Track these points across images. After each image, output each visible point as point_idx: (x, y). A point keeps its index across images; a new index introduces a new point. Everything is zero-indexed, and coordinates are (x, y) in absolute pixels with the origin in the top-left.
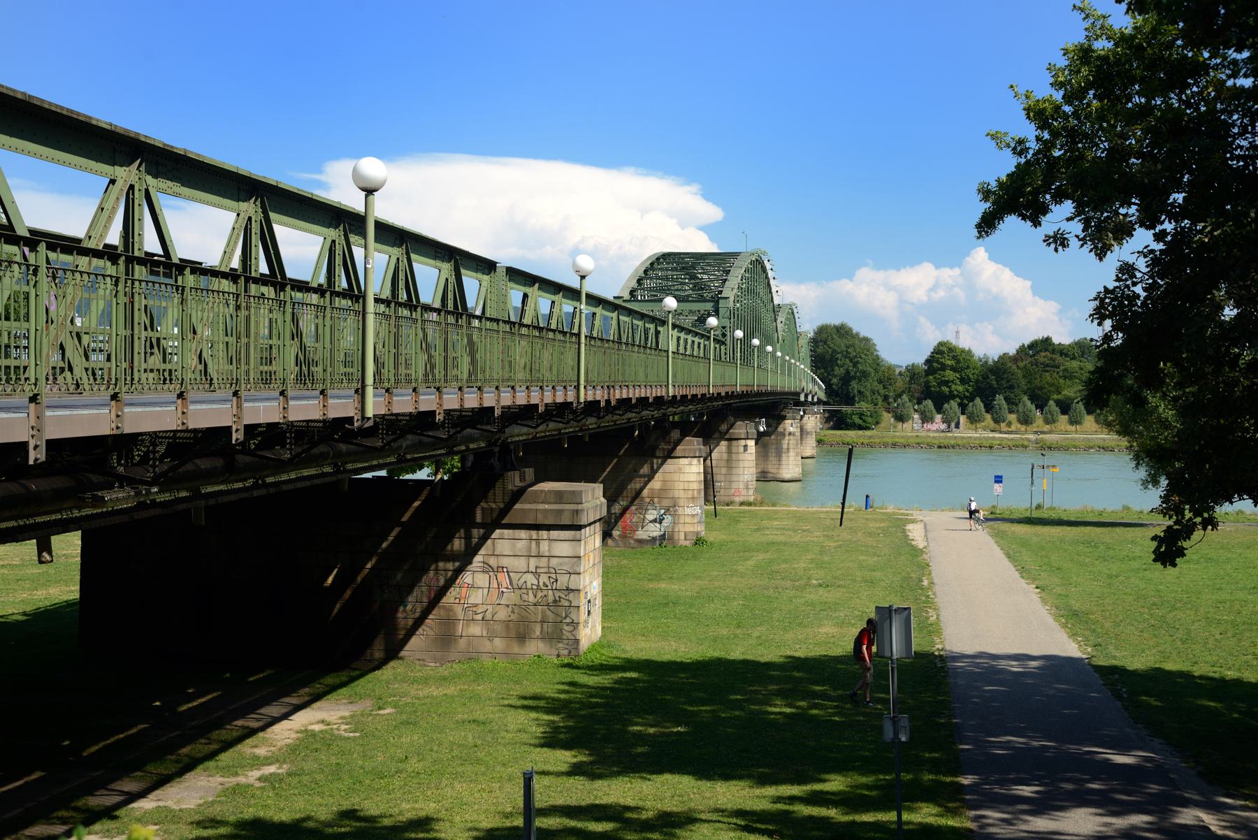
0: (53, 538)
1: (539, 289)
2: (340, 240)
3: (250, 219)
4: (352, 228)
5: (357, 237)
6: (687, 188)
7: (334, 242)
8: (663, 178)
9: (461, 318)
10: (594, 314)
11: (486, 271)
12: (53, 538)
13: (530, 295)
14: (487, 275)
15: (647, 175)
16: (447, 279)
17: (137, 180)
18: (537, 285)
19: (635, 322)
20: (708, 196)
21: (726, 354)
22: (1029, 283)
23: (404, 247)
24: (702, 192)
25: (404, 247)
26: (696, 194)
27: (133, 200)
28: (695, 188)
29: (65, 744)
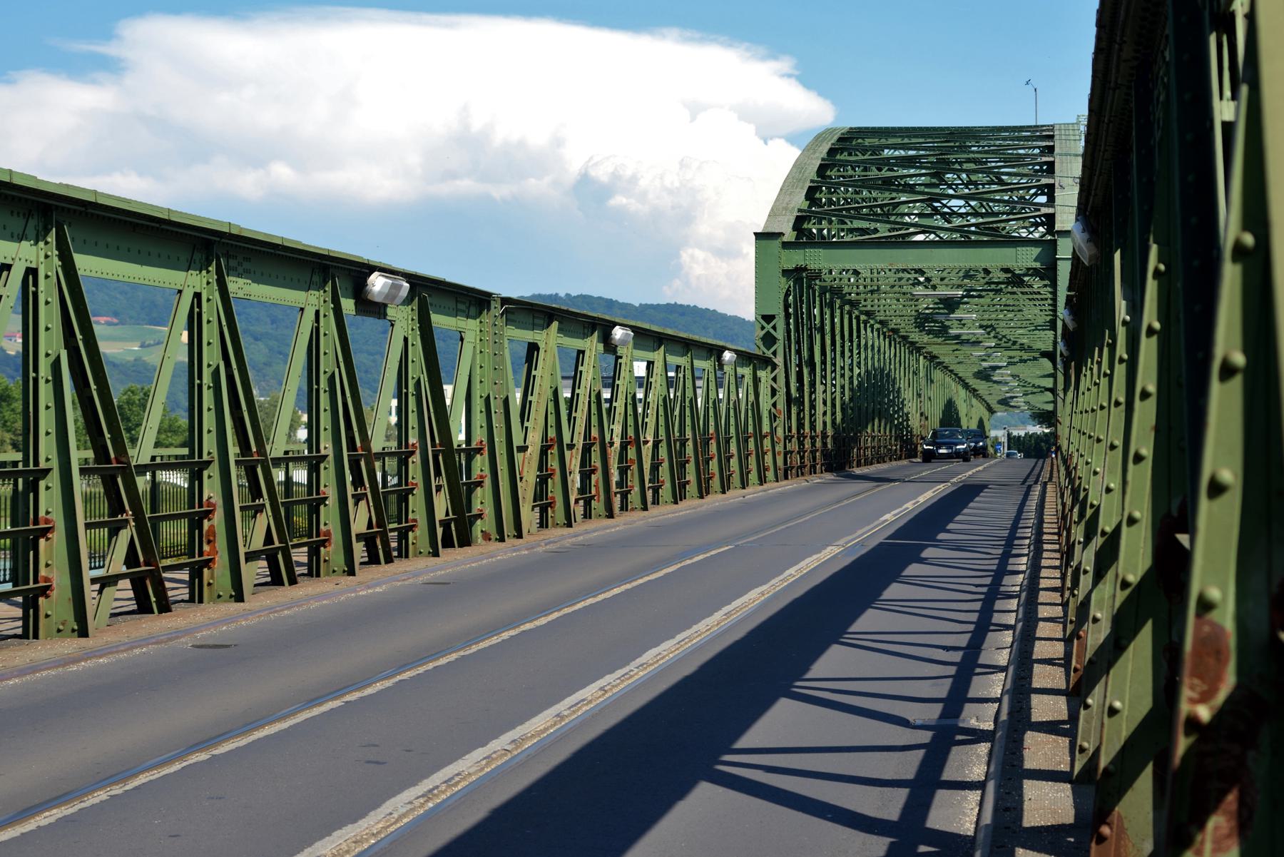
0: (1033, 720)
1: (560, 330)
2: (47, 268)
3: (198, 296)
4: (233, 263)
5: (241, 281)
6: (773, 65)
7: (198, 296)
8: (730, 46)
9: (790, 441)
10: (533, 348)
11: (473, 311)
12: (1033, 720)
13: (542, 345)
14: (475, 318)
15: (701, 41)
16: (406, 340)
17: (42, 259)
18: (555, 325)
19: (697, 363)
20: (808, 78)
21: (774, 392)
23: (212, 268)
24: (797, 73)
25: (328, 288)
26: (790, 76)
27: (36, 295)
28: (785, 64)
29: (1069, 839)
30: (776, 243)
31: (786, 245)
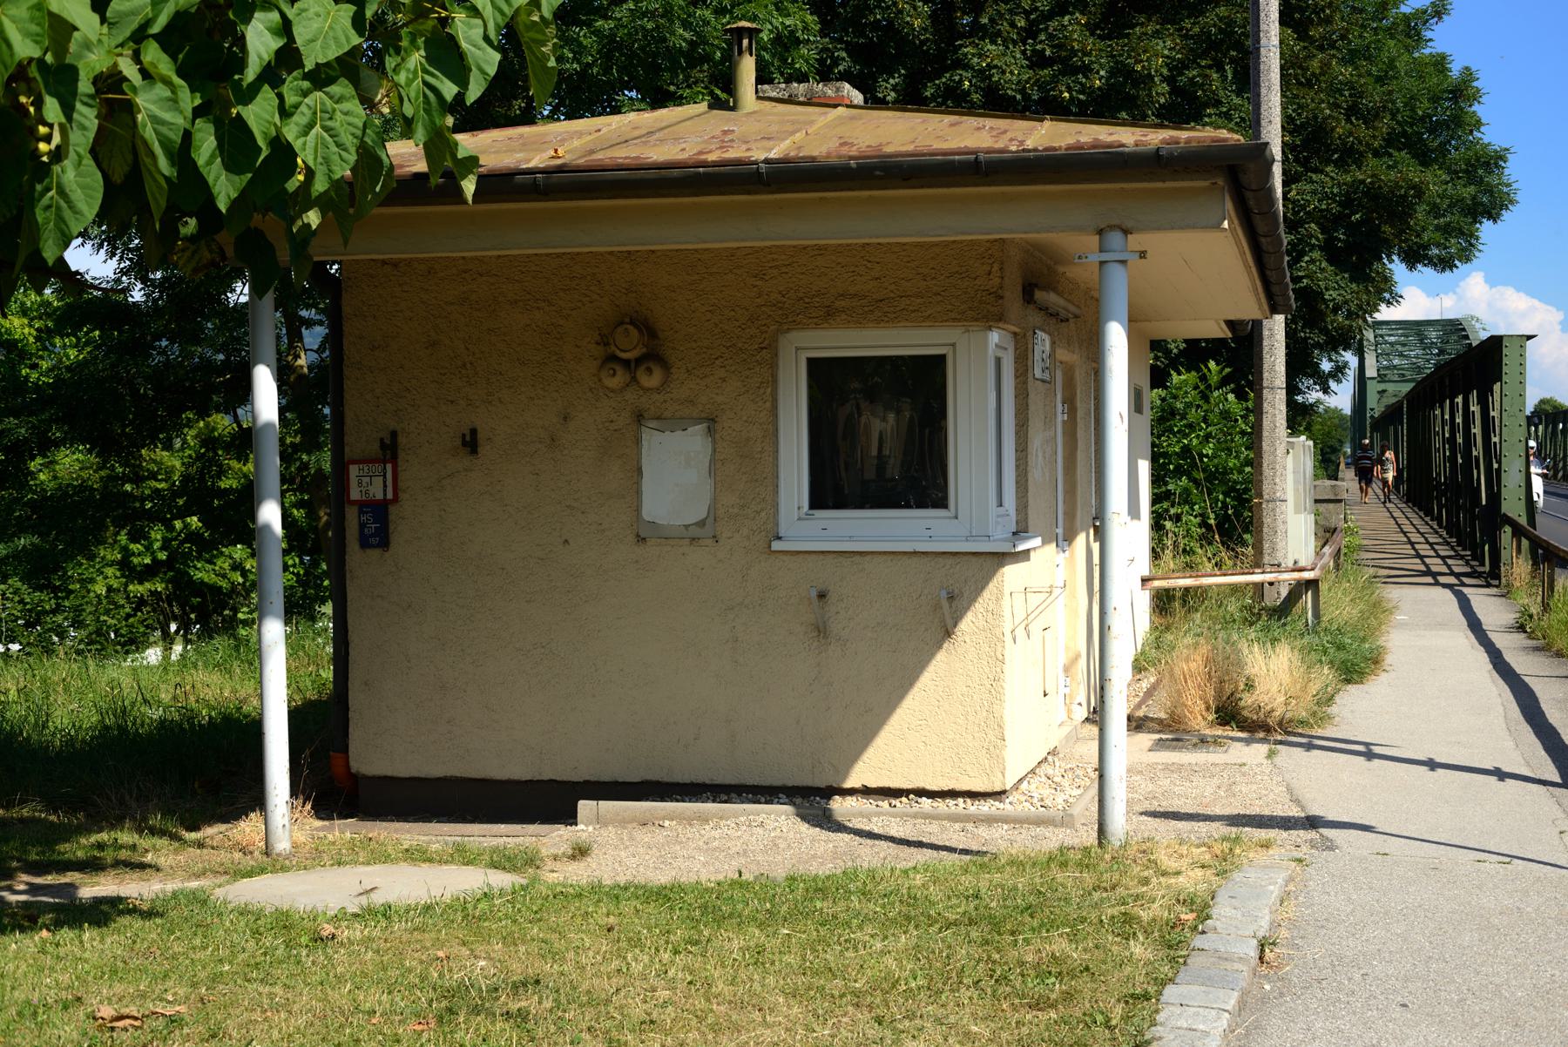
22: (1560, 316)
30: (1375, 381)
31: (1379, 382)
